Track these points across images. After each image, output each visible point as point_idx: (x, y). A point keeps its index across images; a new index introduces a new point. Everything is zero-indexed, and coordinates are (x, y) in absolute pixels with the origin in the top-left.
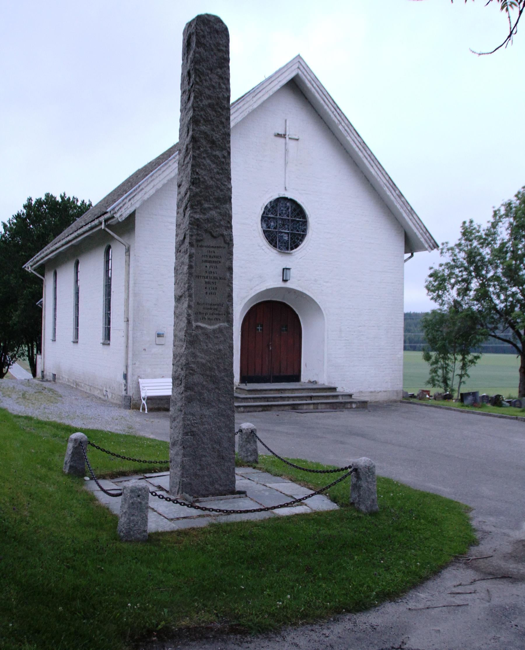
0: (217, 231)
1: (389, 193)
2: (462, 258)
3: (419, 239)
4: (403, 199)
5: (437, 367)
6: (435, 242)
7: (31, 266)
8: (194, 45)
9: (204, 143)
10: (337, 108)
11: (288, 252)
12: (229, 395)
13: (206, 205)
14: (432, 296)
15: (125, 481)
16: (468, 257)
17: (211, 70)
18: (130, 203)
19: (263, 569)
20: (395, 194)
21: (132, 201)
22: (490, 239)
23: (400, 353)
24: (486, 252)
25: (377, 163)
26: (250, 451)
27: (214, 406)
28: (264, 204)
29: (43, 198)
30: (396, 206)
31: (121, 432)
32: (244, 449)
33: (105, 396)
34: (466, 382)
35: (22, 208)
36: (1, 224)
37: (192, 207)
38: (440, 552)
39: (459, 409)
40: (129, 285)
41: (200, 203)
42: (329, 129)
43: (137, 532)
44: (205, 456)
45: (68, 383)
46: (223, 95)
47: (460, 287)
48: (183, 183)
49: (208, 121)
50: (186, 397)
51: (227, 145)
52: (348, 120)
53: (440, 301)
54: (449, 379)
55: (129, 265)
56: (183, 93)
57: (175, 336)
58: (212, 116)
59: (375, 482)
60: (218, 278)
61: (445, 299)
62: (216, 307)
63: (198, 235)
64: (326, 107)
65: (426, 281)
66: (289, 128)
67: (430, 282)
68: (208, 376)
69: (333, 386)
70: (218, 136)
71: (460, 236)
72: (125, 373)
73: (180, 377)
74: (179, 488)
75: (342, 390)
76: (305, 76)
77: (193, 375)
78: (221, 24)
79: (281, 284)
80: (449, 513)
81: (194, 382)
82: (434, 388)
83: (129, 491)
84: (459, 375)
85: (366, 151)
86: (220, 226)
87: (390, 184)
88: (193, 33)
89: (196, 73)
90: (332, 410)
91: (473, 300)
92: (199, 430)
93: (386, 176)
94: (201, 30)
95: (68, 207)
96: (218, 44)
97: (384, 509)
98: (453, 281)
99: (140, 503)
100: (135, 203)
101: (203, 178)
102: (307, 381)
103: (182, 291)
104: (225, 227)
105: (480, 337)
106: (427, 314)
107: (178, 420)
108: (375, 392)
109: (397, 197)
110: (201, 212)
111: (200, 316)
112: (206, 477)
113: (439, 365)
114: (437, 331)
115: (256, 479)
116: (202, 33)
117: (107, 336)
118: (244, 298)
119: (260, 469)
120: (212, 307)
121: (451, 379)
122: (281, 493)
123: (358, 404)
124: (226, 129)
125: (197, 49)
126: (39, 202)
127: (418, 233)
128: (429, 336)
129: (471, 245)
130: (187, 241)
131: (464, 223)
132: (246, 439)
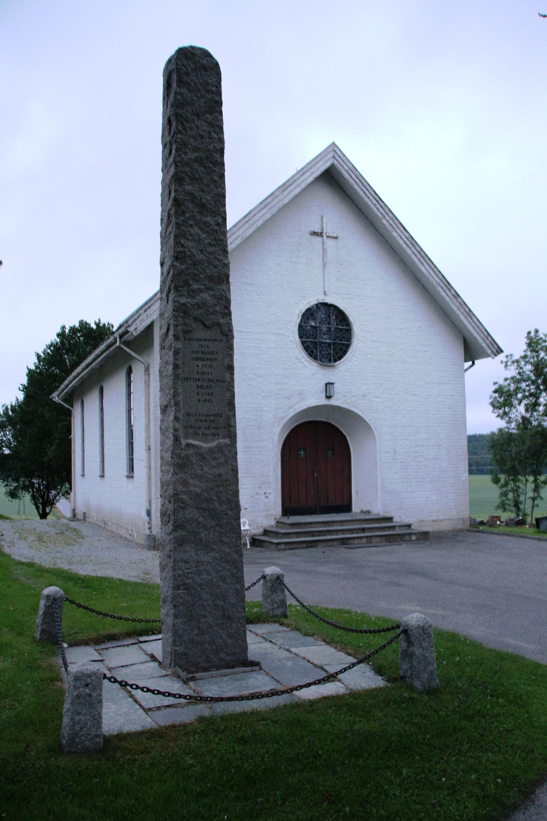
0: (210, 319)
1: (443, 294)
2: (528, 370)
3: (480, 345)
5: (507, 490)
7: (58, 396)
8: (174, 85)
10: (379, 200)
13: (195, 286)
14: (497, 413)
15: (113, 647)
16: (535, 370)
17: (198, 115)
19: (260, 799)
21: (148, 312)
23: (464, 475)
25: (428, 261)
26: (277, 603)
28: (301, 312)
29: (77, 325)
30: (452, 308)
31: (138, 580)
32: (269, 600)
33: (130, 535)
34: (540, 505)
35: (56, 337)
36: (35, 354)
37: (176, 289)
38: (530, 755)
39: (535, 536)
40: (149, 409)
41: (186, 283)
42: (372, 224)
43: (86, 738)
44: (205, 616)
45: (97, 522)
46: (215, 147)
47: (528, 402)
48: (166, 260)
51: (221, 210)
52: (392, 213)
53: (507, 419)
54: (521, 503)
55: (149, 386)
56: (164, 146)
57: (162, 458)
58: (200, 173)
59: (432, 647)
60: (215, 381)
62: (212, 418)
63: (185, 324)
64: (367, 199)
65: (491, 397)
67: (495, 398)
68: (204, 509)
69: (388, 515)
70: (209, 198)
71: (525, 347)
72: (148, 509)
73: (168, 513)
74: (171, 660)
75: (399, 520)
76: (341, 166)
77: (184, 508)
78: (209, 59)
79: (323, 401)
82: (505, 513)
83: (73, 679)
84: (532, 498)
85: (415, 247)
86: (215, 313)
88: (173, 70)
89: (177, 119)
90: (387, 544)
91: (543, 415)
93: (439, 274)
94: (183, 65)
96: (207, 84)
98: (520, 396)
99: (90, 695)
100: (152, 314)
101: (190, 251)
102: (359, 511)
104: (221, 313)
106: (493, 434)
107: (167, 570)
108: (438, 520)
109: (452, 298)
110: (189, 294)
111: (192, 431)
112: (207, 644)
113: (509, 487)
114: (505, 451)
116: (185, 70)
117: (131, 468)
118: (282, 419)
119: (288, 626)
120: (208, 418)
121: (524, 503)
123: (419, 536)
124: (219, 190)
125: (179, 89)
126: (73, 330)
127: (478, 338)
128: (497, 457)
129: (538, 357)
130: (171, 333)
131: (529, 333)
132: (271, 587)
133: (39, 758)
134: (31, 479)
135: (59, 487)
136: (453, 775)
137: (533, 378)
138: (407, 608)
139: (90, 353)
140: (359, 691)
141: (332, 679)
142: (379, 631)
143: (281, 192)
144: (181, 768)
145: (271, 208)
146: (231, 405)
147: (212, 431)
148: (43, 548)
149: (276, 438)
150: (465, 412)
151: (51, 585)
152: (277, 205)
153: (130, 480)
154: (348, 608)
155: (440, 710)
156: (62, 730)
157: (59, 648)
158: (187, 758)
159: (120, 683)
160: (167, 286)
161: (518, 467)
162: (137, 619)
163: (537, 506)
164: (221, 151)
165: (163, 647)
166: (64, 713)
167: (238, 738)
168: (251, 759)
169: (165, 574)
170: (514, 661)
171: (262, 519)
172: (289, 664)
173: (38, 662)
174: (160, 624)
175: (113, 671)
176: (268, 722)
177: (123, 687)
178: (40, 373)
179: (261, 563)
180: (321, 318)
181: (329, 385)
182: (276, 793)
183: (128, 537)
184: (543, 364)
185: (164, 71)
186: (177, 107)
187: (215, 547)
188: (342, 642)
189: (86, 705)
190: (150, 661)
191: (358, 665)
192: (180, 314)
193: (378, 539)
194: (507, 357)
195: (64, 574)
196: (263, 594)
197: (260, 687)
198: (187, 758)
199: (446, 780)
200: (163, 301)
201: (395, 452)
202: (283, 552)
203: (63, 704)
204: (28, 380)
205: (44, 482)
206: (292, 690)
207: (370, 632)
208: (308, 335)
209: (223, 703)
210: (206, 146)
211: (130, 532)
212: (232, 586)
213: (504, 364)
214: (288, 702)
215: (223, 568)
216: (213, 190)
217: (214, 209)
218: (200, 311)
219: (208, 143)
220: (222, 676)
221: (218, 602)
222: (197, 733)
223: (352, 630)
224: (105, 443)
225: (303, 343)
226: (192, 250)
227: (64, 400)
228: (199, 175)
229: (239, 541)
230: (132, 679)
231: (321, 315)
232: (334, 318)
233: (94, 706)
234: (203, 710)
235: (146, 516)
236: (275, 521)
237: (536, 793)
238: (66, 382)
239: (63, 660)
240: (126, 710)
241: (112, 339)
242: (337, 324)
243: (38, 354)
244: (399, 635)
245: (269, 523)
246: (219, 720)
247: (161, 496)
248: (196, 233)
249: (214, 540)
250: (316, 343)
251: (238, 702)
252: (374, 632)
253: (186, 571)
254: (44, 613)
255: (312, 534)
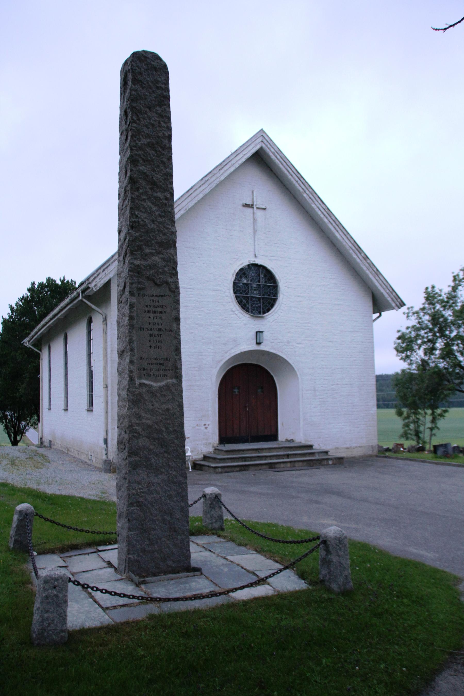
0: (160, 278)
1: (355, 256)
2: (427, 320)
4: (368, 261)
5: (409, 422)
6: (402, 301)
7: (29, 341)
8: (130, 83)
9: (144, 184)
10: (300, 177)
11: (261, 316)
12: (180, 459)
13: (147, 251)
15: (75, 555)
17: (149, 108)
18: (104, 273)
19: (201, 685)
20: (360, 257)
22: (451, 302)
23: (373, 409)
24: (448, 314)
25: (342, 228)
26: (215, 518)
27: (164, 472)
28: (235, 271)
29: (45, 282)
31: (96, 498)
32: (209, 516)
33: (90, 460)
34: (437, 434)
35: (27, 292)
36: (9, 306)
37: (132, 253)
40: (106, 353)
41: (140, 248)
42: (295, 198)
43: (53, 632)
44: (154, 529)
45: (61, 449)
46: (164, 134)
47: (426, 347)
48: (123, 228)
49: (148, 160)
50: (130, 463)
51: (169, 186)
52: (311, 188)
53: (409, 361)
54: (421, 432)
55: (106, 334)
56: (121, 134)
57: (119, 395)
58: (152, 156)
59: (347, 555)
60: (164, 330)
61: (414, 359)
62: (162, 362)
63: (139, 282)
64: (290, 177)
65: (395, 343)
66: (256, 199)
67: (399, 344)
68: (154, 439)
69: (309, 443)
70: (159, 177)
71: (423, 300)
72: (105, 438)
73: (124, 441)
74: (126, 566)
76: (269, 149)
77: (137, 438)
78: (159, 61)
79: (255, 347)
80: (437, 587)
81: (139, 446)
83: (42, 582)
85: (330, 217)
86: (164, 273)
87: (355, 247)
88: (129, 70)
89: (132, 111)
90: (306, 467)
91: (439, 358)
92: (146, 500)
93: (351, 240)
95: (67, 289)
96: (157, 82)
97: (360, 585)
98: (419, 342)
99: (57, 596)
101: (143, 221)
102: (284, 440)
103: (123, 345)
104: (170, 273)
105: (448, 392)
106: (397, 374)
107: (123, 489)
108: (351, 447)
109: (363, 259)
110: (142, 258)
111: (144, 372)
114: (407, 388)
115: (218, 550)
116: (139, 70)
117: (91, 403)
118: (219, 362)
119: (224, 537)
120: (158, 362)
122: (242, 568)
123: (335, 461)
124: (167, 170)
125: (134, 86)
126: (41, 285)
127: (385, 293)
129: (434, 308)
130: (127, 289)
131: (427, 288)
132: (210, 504)
133: (13, 650)
134: (5, 411)
135: (28, 419)
136: (365, 664)
137: (431, 326)
138: (326, 521)
139: (56, 305)
140: (285, 592)
141: (262, 582)
142: (302, 542)
143: (218, 170)
144: (134, 658)
145: (210, 184)
146: (178, 351)
147: (162, 372)
148: (15, 471)
149: (214, 378)
150: (373, 356)
151: (23, 502)
152: (215, 181)
153: (90, 413)
154: (276, 522)
155: (354, 609)
156: (33, 626)
157: (30, 556)
158: (140, 650)
159: (83, 586)
160: (124, 250)
161: (418, 402)
162: (96, 531)
163: (435, 435)
164: (169, 138)
165: (118, 556)
166: (34, 611)
167: (183, 633)
168: (194, 651)
169: (120, 493)
170: (416, 567)
171: (202, 446)
172: (226, 570)
173: (11, 567)
174: (116, 536)
175: (75, 576)
176: (208, 619)
177: (85, 589)
178: (13, 322)
179: (202, 484)
180: (252, 276)
181: (259, 333)
182: (215, 680)
183: (88, 461)
184: (439, 315)
185: (121, 71)
186: (132, 100)
187: (164, 470)
188: (270, 551)
189: (53, 604)
190: (107, 567)
191: (284, 571)
192: (134, 273)
193: (300, 463)
194: (408, 308)
195: (33, 493)
196: (203, 511)
197: (199, 589)
198: (140, 650)
199: (359, 669)
200: (120, 263)
201: (315, 390)
202: (220, 475)
203: (34, 604)
204: (2, 328)
205: (16, 415)
206: (229, 591)
207: (294, 542)
208: (241, 291)
209: (170, 602)
210: (157, 133)
211: (90, 457)
212: (178, 503)
213: (406, 315)
214: (225, 602)
215: (171, 489)
216: (162, 170)
217: (163, 186)
218: (151, 272)
219: (158, 131)
220: (168, 580)
221: (166, 517)
222: (148, 628)
223: (279, 541)
224: (69, 382)
225: (237, 297)
226: (145, 220)
227: (34, 345)
228: (150, 157)
229: (184, 465)
230: (92, 582)
231: (252, 273)
232: (263, 276)
233: (61, 605)
234: (153, 609)
235: (103, 444)
236: (214, 448)
237: (436, 680)
238: (36, 330)
239: (33, 566)
240: (87, 609)
241: (75, 293)
242: (265, 282)
243: (11, 306)
244: (319, 545)
245: (208, 450)
246: (166, 617)
247: (118, 427)
248: (148, 206)
249: (163, 465)
250: (248, 297)
251: (182, 602)
252: (298, 542)
253: (139, 491)
254: (17, 526)
255: (244, 459)
